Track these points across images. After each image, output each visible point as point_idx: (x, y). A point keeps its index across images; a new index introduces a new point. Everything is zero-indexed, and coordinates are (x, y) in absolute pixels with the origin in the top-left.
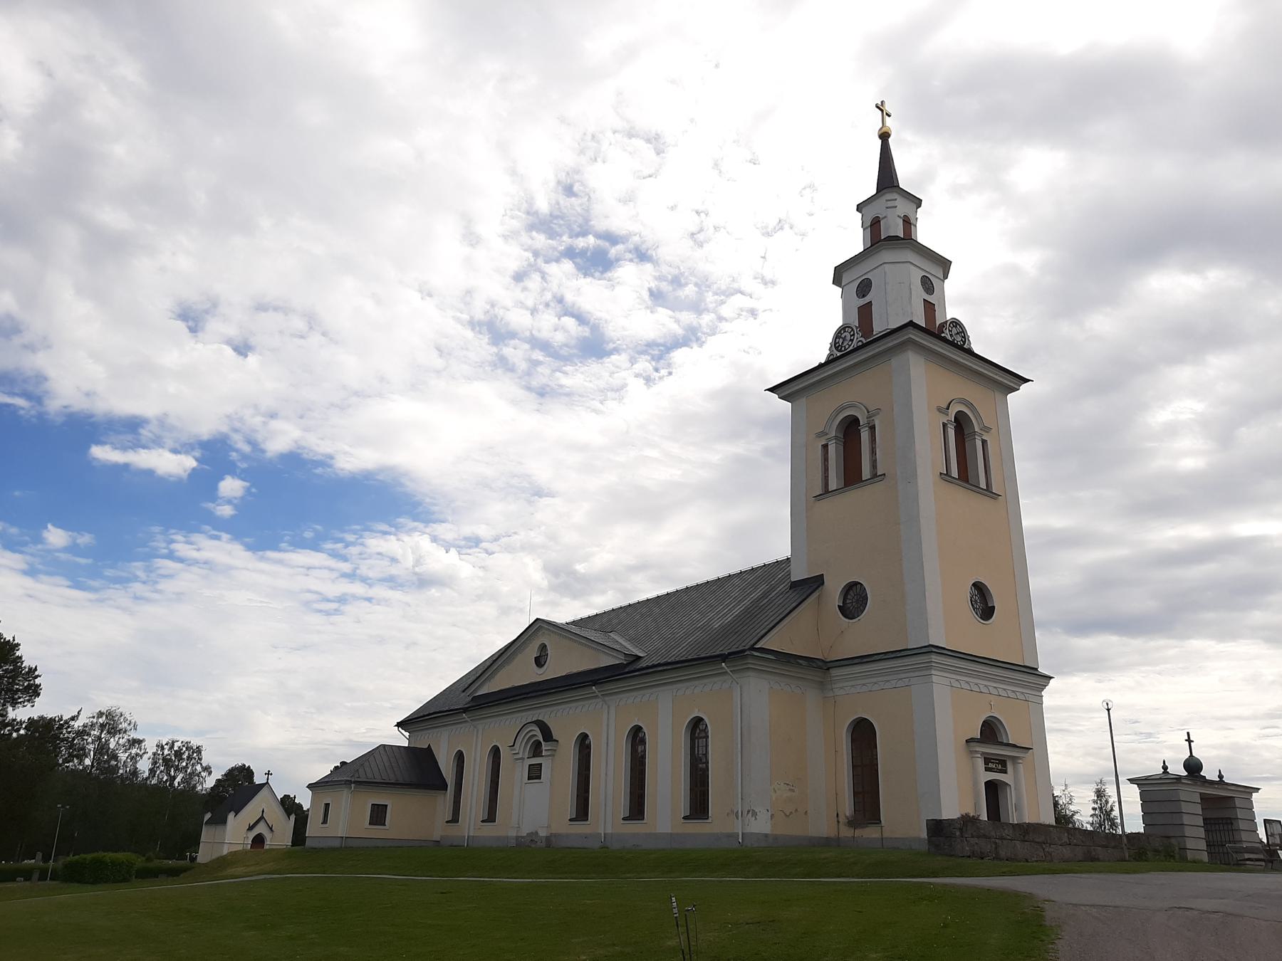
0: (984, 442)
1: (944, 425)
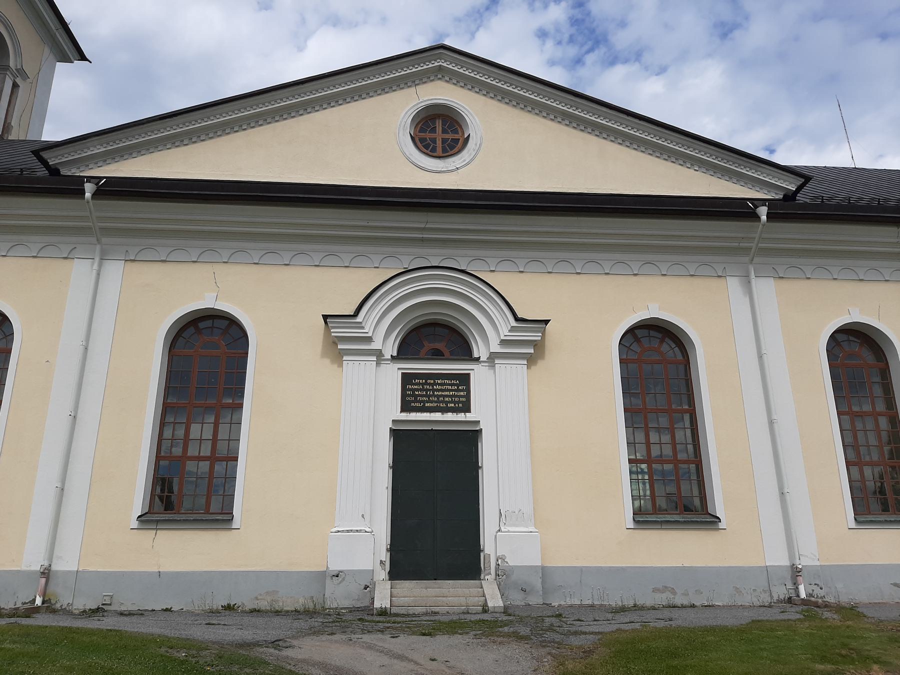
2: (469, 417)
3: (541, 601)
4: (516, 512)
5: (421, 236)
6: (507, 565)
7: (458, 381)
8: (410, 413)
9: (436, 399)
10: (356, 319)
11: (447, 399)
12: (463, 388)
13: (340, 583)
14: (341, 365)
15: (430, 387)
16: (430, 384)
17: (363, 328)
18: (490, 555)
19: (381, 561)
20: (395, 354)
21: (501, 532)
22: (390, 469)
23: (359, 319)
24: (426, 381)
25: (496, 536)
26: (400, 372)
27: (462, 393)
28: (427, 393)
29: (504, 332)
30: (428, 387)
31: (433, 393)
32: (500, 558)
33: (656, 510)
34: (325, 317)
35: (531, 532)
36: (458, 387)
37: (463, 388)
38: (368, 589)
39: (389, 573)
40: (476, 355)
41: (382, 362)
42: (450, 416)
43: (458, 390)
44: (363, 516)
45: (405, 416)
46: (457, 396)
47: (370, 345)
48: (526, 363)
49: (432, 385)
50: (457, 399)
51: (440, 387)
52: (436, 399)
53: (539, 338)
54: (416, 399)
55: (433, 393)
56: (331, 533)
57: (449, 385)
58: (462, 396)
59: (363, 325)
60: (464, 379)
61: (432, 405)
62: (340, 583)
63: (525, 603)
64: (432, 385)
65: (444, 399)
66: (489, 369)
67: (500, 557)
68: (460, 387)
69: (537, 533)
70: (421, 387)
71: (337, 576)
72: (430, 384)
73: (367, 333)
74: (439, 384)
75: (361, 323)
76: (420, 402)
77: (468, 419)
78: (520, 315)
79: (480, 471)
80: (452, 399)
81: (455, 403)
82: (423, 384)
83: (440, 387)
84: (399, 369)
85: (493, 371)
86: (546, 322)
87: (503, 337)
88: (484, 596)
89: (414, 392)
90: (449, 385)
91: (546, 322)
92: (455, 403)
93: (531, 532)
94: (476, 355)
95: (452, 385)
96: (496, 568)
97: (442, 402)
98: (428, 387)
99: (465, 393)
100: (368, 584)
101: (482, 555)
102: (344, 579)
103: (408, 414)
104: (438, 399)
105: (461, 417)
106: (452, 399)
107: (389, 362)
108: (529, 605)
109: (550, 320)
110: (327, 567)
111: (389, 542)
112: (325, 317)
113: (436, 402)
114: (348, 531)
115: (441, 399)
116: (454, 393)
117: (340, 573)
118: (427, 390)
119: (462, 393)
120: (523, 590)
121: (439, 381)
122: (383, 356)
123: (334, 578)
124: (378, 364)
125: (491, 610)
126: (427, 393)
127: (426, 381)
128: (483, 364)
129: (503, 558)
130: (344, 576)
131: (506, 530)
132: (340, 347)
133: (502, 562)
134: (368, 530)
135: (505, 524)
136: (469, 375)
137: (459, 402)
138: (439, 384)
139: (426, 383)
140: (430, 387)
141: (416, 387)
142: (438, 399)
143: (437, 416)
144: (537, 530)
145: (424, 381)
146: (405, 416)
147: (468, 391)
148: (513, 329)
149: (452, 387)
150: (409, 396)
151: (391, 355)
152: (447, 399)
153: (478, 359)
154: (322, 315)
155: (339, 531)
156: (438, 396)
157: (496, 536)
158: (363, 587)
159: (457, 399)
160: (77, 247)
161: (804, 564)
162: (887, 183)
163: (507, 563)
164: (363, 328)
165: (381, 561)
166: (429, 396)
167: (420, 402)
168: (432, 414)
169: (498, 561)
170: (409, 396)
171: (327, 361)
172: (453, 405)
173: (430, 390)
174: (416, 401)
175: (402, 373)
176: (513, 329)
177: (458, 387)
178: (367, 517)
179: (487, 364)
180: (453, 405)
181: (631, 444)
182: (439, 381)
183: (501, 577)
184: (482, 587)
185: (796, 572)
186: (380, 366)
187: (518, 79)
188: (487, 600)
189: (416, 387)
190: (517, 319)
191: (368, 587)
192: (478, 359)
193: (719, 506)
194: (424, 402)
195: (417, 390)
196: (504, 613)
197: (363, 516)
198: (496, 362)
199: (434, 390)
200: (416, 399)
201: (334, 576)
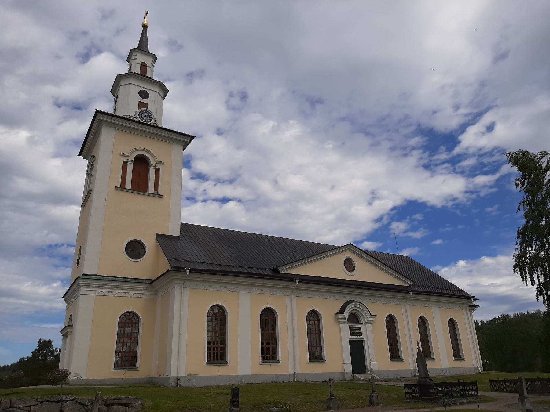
0: (157, 170)
1: (125, 163)
2: (362, 337)
29: (369, 318)
33: (118, 366)
34: (115, 187)
45: (351, 337)
60: (360, 328)
143: (356, 337)
146: (351, 337)
148: (370, 317)
153: (362, 323)
156: (356, 332)
160: (137, 55)
161: (9, 406)
162: (314, 246)
168: (352, 336)
181: (208, 326)
185: (295, 374)
190: (371, 315)
192: (362, 323)
193: (326, 356)
196: (426, 360)
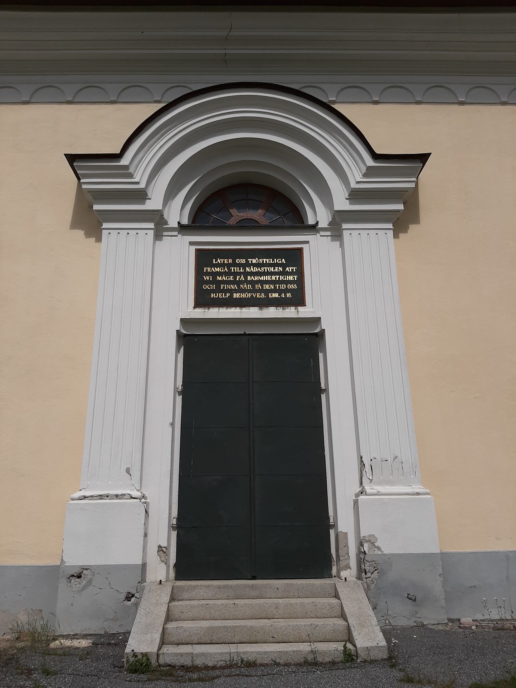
2: (303, 312)
3: (443, 618)
4: (389, 460)
5: (223, 52)
6: (379, 552)
7: (283, 260)
8: (209, 309)
9: (250, 287)
10: (119, 162)
11: (267, 287)
12: (292, 270)
13: (83, 589)
14: (99, 239)
15: (240, 269)
16: (240, 265)
17: (131, 176)
18: (346, 533)
19: (160, 547)
20: (185, 221)
21: (366, 495)
22: (179, 395)
23: (125, 161)
24: (234, 261)
25: (356, 503)
26: (193, 248)
27: (291, 278)
28: (235, 278)
30: (237, 269)
31: (246, 278)
32: (367, 541)
34: (72, 158)
35: (418, 494)
36: (284, 269)
37: (292, 270)
38: (133, 599)
39: (175, 566)
40: (311, 221)
41: (165, 234)
42: (272, 312)
43: (284, 273)
44: (128, 471)
45: (201, 313)
46: (283, 282)
47: (144, 204)
48: (392, 227)
49: (244, 266)
50: (283, 287)
51: (256, 270)
52: (250, 287)
53: (413, 185)
54: (218, 287)
55: (246, 278)
56: (73, 500)
57: (270, 265)
58: (290, 282)
59: (131, 170)
61: (244, 296)
62: (83, 589)
63: (415, 622)
64: (244, 266)
65: (262, 287)
66: (332, 241)
67: (367, 539)
68: (287, 269)
69: (429, 496)
70: (226, 269)
71: (79, 577)
72: (240, 265)
73: (138, 183)
74: (254, 265)
75: (126, 167)
76: (225, 291)
77: (301, 315)
78: (378, 151)
79: (323, 397)
80: (275, 287)
81: (280, 292)
82: (229, 266)
83: (256, 270)
84: (191, 243)
85: (338, 243)
86: (423, 158)
87: (353, 185)
88: (343, 616)
89: (214, 278)
90: (270, 265)
91: (423, 158)
92: (280, 292)
93: (418, 494)
94: (311, 221)
95: (274, 265)
96: (358, 555)
97: (260, 291)
98: (237, 269)
99: (296, 277)
100: (133, 591)
101: (332, 532)
102: (90, 582)
103: (207, 310)
104: (253, 286)
105: (290, 312)
106: (275, 287)
107: (176, 233)
108: (423, 625)
109: (431, 153)
110: (62, 560)
111: (175, 512)
112: (72, 158)
113: (249, 291)
114: (101, 497)
115: (258, 286)
116: (277, 277)
117: (85, 572)
118: (235, 274)
119: (291, 278)
120: (410, 599)
121: (254, 261)
122: (166, 223)
123: (73, 580)
124: (158, 236)
125: (363, 655)
126: (235, 278)
127: (234, 261)
128: (322, 233)
129: (372, 541)
130: (89, 577)
131: (375, 491)
132: (96, 207)
133: (370, 549)
134: (135, 494)
135: (371, 481)
136: (300, 250)
137: (287, 291)
138: (254, 265)
139: (234, 264)
140: (240, 269)
141: (218, 270)
142: (253, 286)
144: (428, 491)
145: (230, 261)
146: (201, 313)
147: (300, 273)
149: (274, 269)
150: (208, 282)
151: (179, 223)
152: (267, 287)
154: (65, 154)
155: (85, 497)
156: (253, 283)
157: (356, 503)
158: (123, 596)
159: (283, 287)
163: (379, 548)
164: (131, 176)
165: (160, 547)
166: (239, 283)
167: (225, 291)
168: (245, 310)
169: (362, 545)
170: (208, 282)
171: (80, 233)
172: (276, 295)
173: (240, 274)
174: (218, 290)
175: (196, 249)
176: (370, 172)
177: (284, 269)
178: (136, 472)
179: (329, 233)
180: (276, 295)
182: (254, 261)
183: (369, 575)
184: (337, 596)
186: (161, 240)
187: (233, 648)
188: (352, 629)
189: (218, 270)
190: (376, 156)
191: (133, 596)
194: (231, 291)
195: (220, 274)
197: (128, 471)
198: (344, 226)
199: (246, 274)
200: (218, 287)
201: (73, 576)
